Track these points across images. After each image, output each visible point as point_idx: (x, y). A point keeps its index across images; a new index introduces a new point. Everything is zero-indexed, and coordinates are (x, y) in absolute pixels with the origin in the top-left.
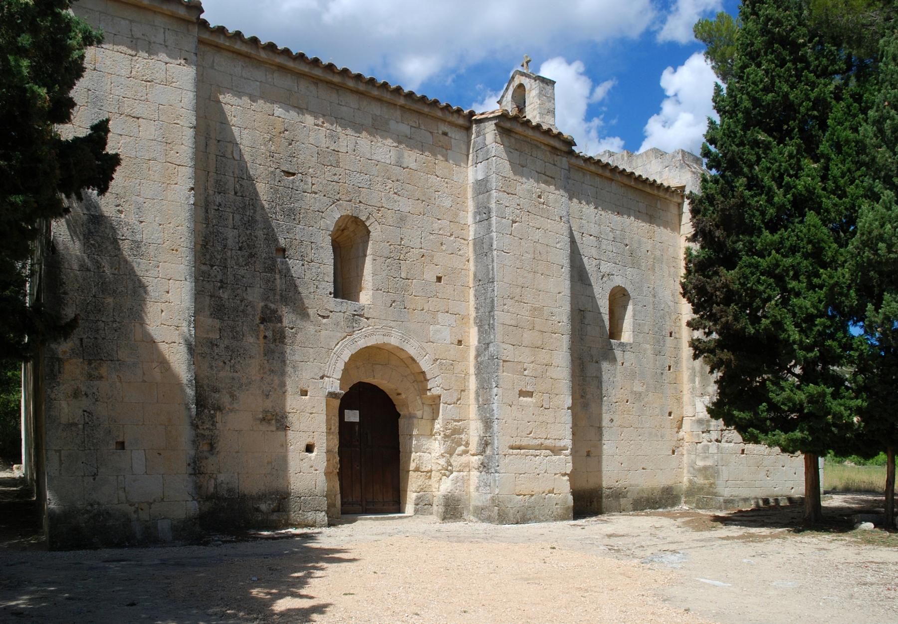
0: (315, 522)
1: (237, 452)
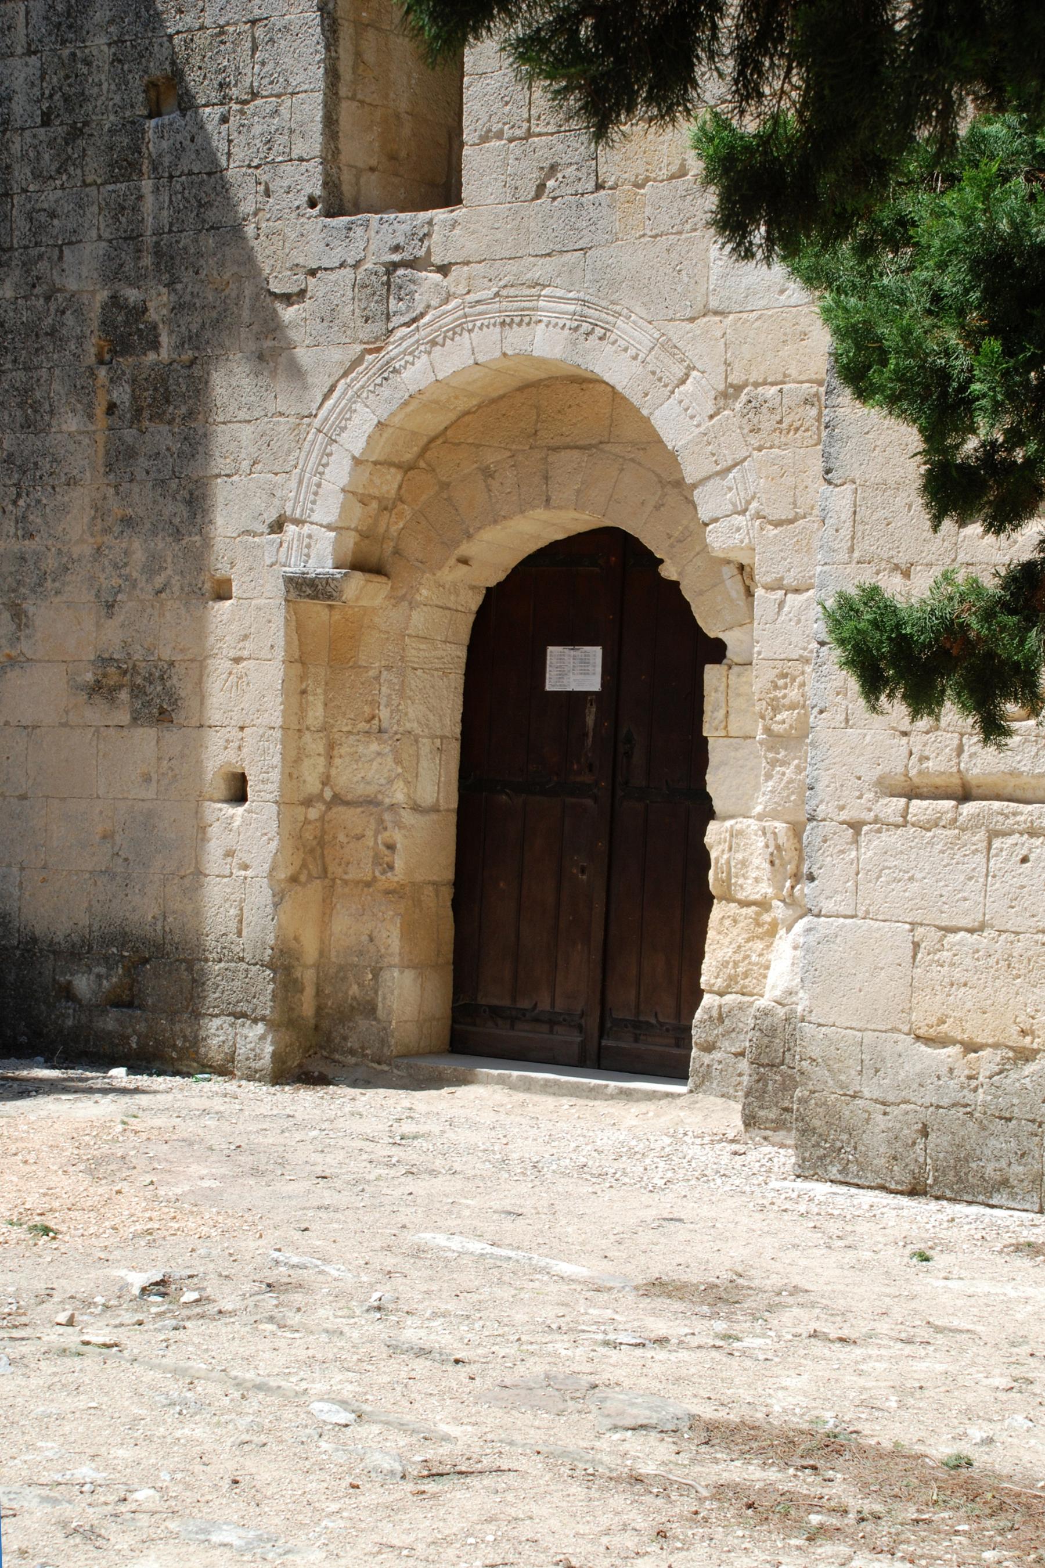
0: (231, 1058)
1: (23, 797)
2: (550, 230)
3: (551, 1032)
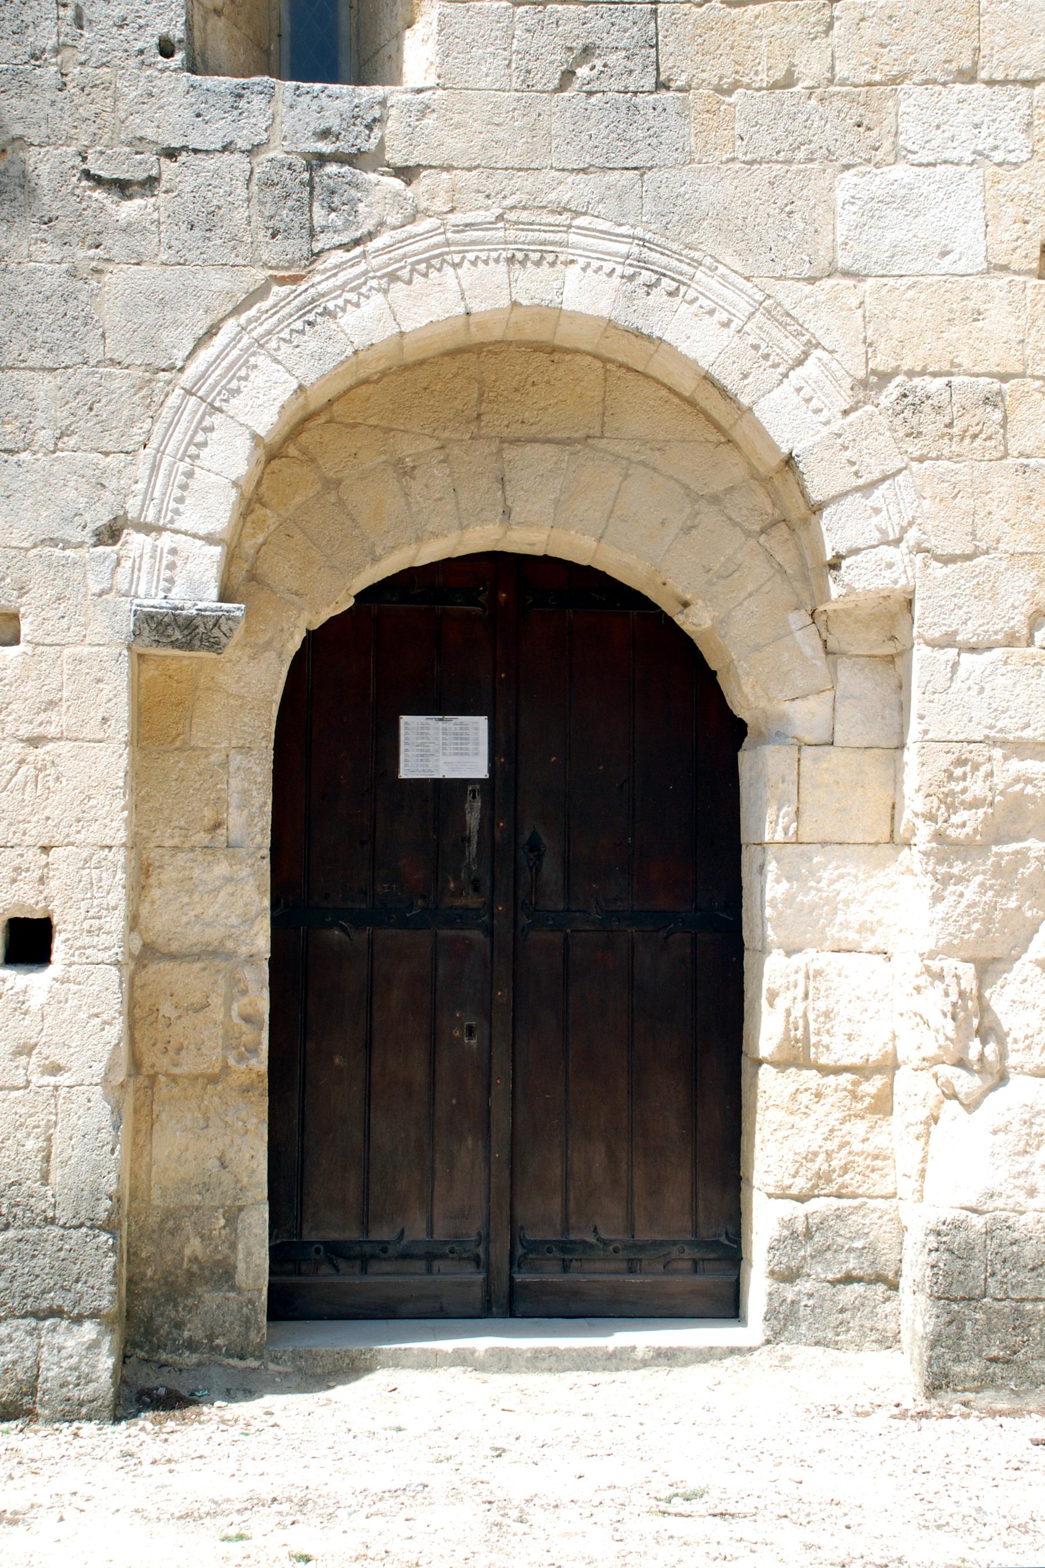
2: (584, 137)
3: (429, 1271)
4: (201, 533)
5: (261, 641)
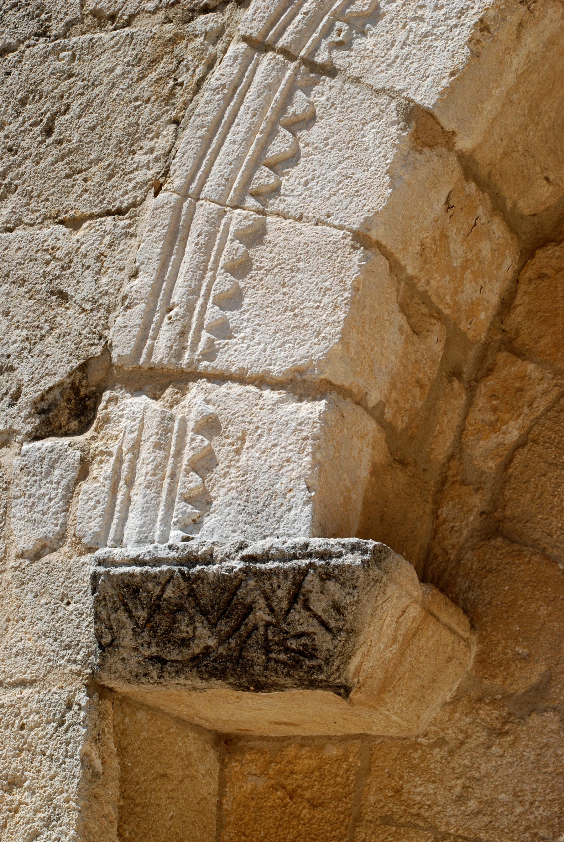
4: (277, 369)
5: (519, 687)
